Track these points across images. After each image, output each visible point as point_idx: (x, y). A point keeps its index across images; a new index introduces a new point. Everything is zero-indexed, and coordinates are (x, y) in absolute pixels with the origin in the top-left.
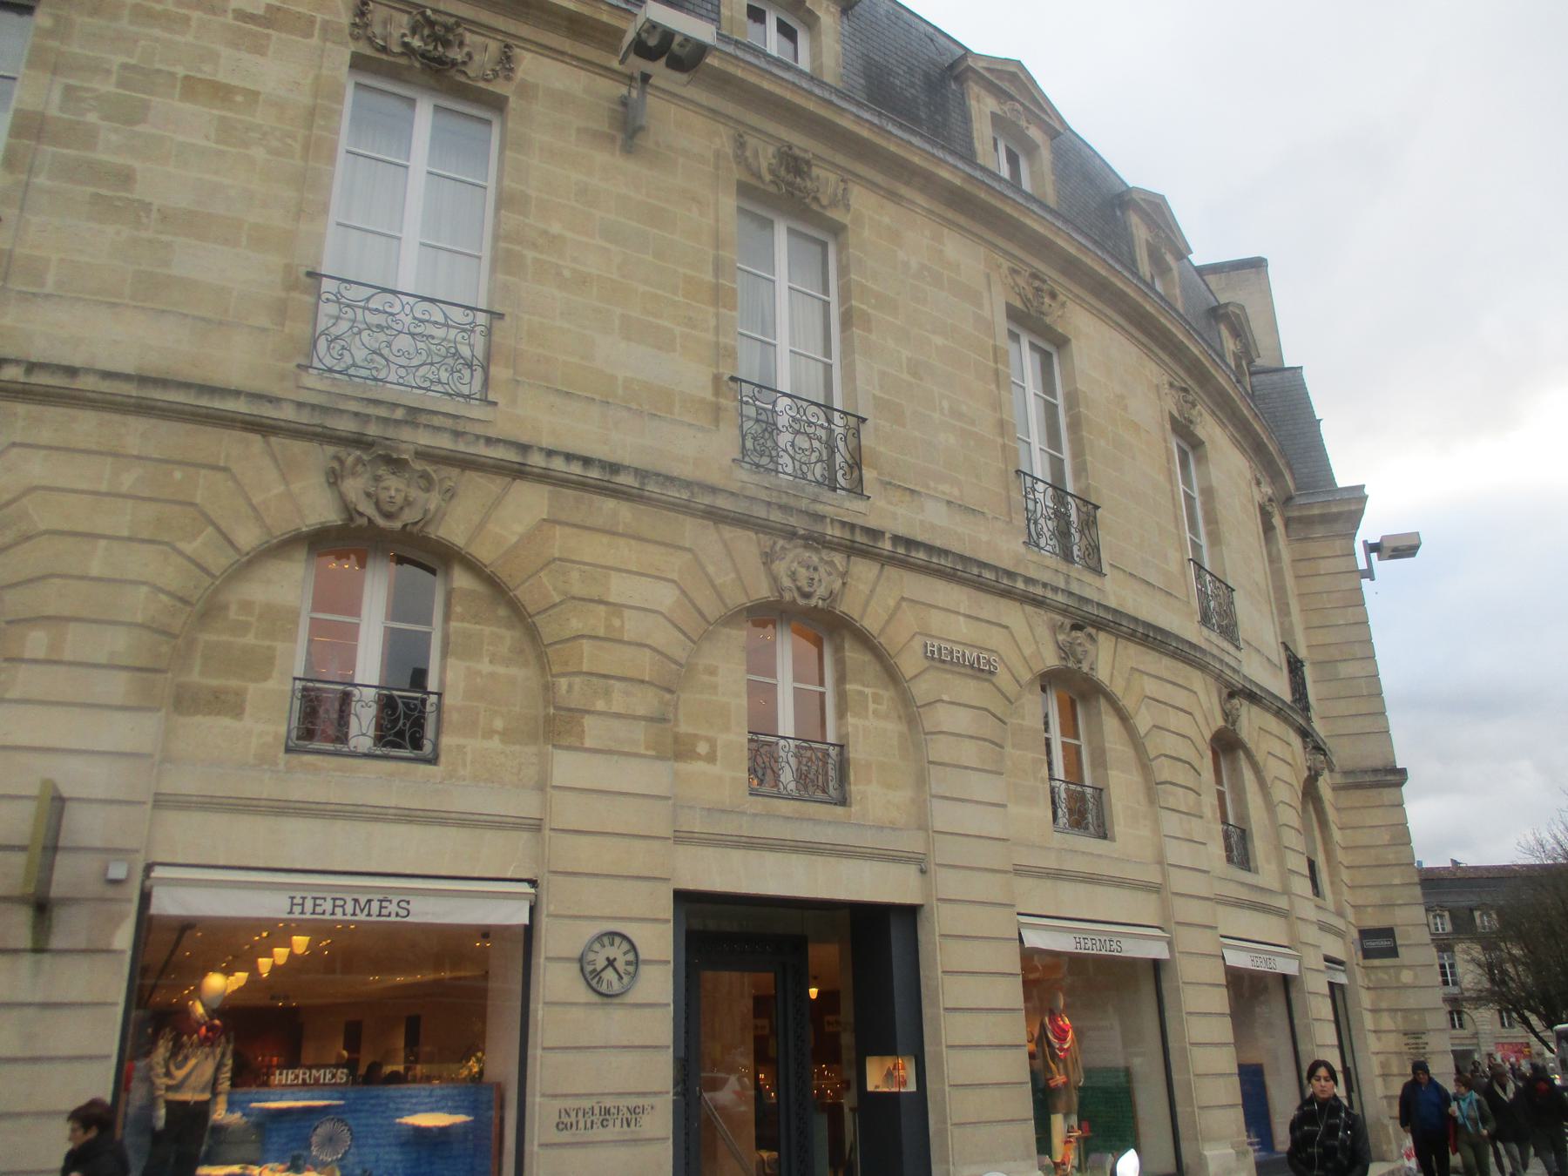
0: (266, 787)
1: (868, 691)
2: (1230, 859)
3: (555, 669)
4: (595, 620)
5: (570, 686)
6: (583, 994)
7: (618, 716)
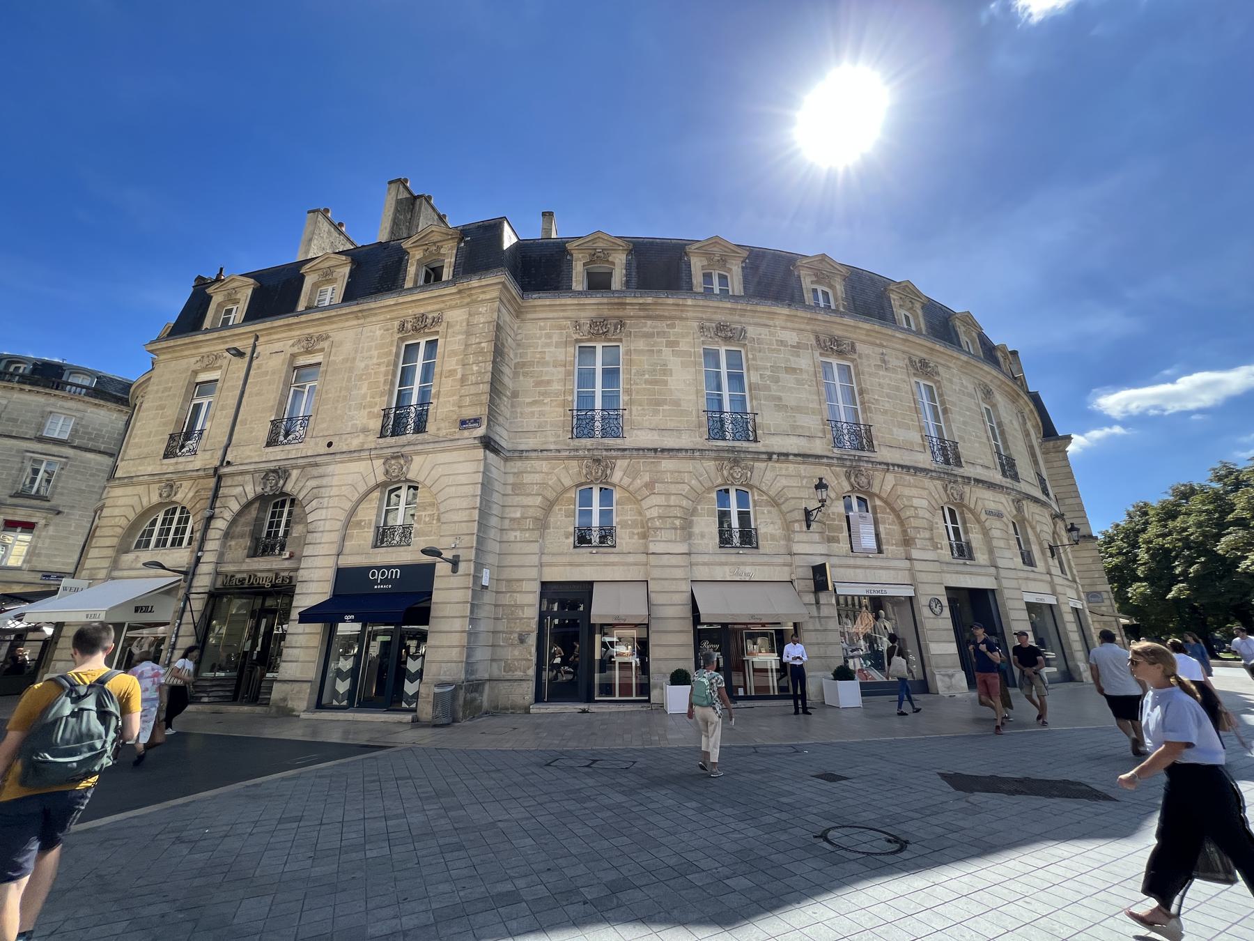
2: (1024, 563)
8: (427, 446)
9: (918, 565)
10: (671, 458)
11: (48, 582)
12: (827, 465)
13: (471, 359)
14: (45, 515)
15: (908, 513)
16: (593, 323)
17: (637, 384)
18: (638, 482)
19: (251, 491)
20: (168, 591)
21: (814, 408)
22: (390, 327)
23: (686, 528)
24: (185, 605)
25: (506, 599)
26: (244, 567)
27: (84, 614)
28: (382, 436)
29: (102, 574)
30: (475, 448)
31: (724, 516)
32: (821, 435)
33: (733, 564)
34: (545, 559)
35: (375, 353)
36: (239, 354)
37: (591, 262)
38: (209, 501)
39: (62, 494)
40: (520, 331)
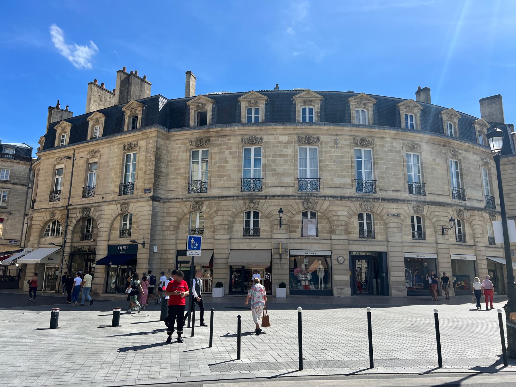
4: (336, 218)
8: (133, 200)
9: (334, 242)
10: (225, 200)
11: (12, 244)
12: (293, 199)
13: (148, 163)
14: (6, 215)
16: (196, 142)
17: (214, 168)
18: (212, 211)
19: (79, 215)
20: (57, 252)
21: (291, 173)
22: (120, 147)
23: (230, 228)
24: (63, 257)
25: (164, 257)
26: (80, 244)
27: (34, 261)
29: (36, 246)
30: (149, 201)
31: (248, 223)
33: (247, 243)
34: (178, 241)
35: (115, 159)
36: (69, 158)
37: (198, 109)
38: (66, 219)
39: (11, 205)
40: (169, 146)
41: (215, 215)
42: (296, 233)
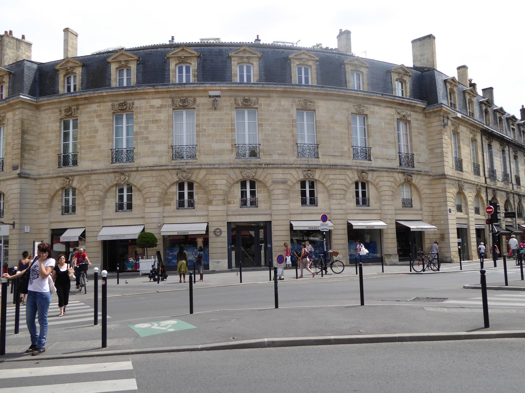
0: (174, 214)
1: (262, 189)
3: (208, 195)
4: (214, 187)
5: (211, 197)
6: (214, 236)
7: (218, 200)
15: (211, 188)
17: (83, 139)
28: (60, 167)
31: (121, 198)
32: (166, 154)
41: (85, 190)
42: (171, 206)
